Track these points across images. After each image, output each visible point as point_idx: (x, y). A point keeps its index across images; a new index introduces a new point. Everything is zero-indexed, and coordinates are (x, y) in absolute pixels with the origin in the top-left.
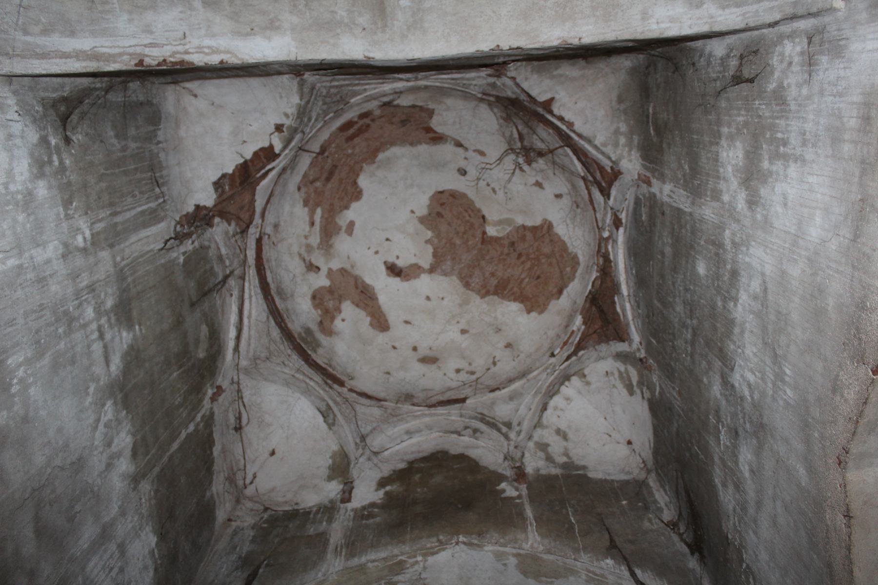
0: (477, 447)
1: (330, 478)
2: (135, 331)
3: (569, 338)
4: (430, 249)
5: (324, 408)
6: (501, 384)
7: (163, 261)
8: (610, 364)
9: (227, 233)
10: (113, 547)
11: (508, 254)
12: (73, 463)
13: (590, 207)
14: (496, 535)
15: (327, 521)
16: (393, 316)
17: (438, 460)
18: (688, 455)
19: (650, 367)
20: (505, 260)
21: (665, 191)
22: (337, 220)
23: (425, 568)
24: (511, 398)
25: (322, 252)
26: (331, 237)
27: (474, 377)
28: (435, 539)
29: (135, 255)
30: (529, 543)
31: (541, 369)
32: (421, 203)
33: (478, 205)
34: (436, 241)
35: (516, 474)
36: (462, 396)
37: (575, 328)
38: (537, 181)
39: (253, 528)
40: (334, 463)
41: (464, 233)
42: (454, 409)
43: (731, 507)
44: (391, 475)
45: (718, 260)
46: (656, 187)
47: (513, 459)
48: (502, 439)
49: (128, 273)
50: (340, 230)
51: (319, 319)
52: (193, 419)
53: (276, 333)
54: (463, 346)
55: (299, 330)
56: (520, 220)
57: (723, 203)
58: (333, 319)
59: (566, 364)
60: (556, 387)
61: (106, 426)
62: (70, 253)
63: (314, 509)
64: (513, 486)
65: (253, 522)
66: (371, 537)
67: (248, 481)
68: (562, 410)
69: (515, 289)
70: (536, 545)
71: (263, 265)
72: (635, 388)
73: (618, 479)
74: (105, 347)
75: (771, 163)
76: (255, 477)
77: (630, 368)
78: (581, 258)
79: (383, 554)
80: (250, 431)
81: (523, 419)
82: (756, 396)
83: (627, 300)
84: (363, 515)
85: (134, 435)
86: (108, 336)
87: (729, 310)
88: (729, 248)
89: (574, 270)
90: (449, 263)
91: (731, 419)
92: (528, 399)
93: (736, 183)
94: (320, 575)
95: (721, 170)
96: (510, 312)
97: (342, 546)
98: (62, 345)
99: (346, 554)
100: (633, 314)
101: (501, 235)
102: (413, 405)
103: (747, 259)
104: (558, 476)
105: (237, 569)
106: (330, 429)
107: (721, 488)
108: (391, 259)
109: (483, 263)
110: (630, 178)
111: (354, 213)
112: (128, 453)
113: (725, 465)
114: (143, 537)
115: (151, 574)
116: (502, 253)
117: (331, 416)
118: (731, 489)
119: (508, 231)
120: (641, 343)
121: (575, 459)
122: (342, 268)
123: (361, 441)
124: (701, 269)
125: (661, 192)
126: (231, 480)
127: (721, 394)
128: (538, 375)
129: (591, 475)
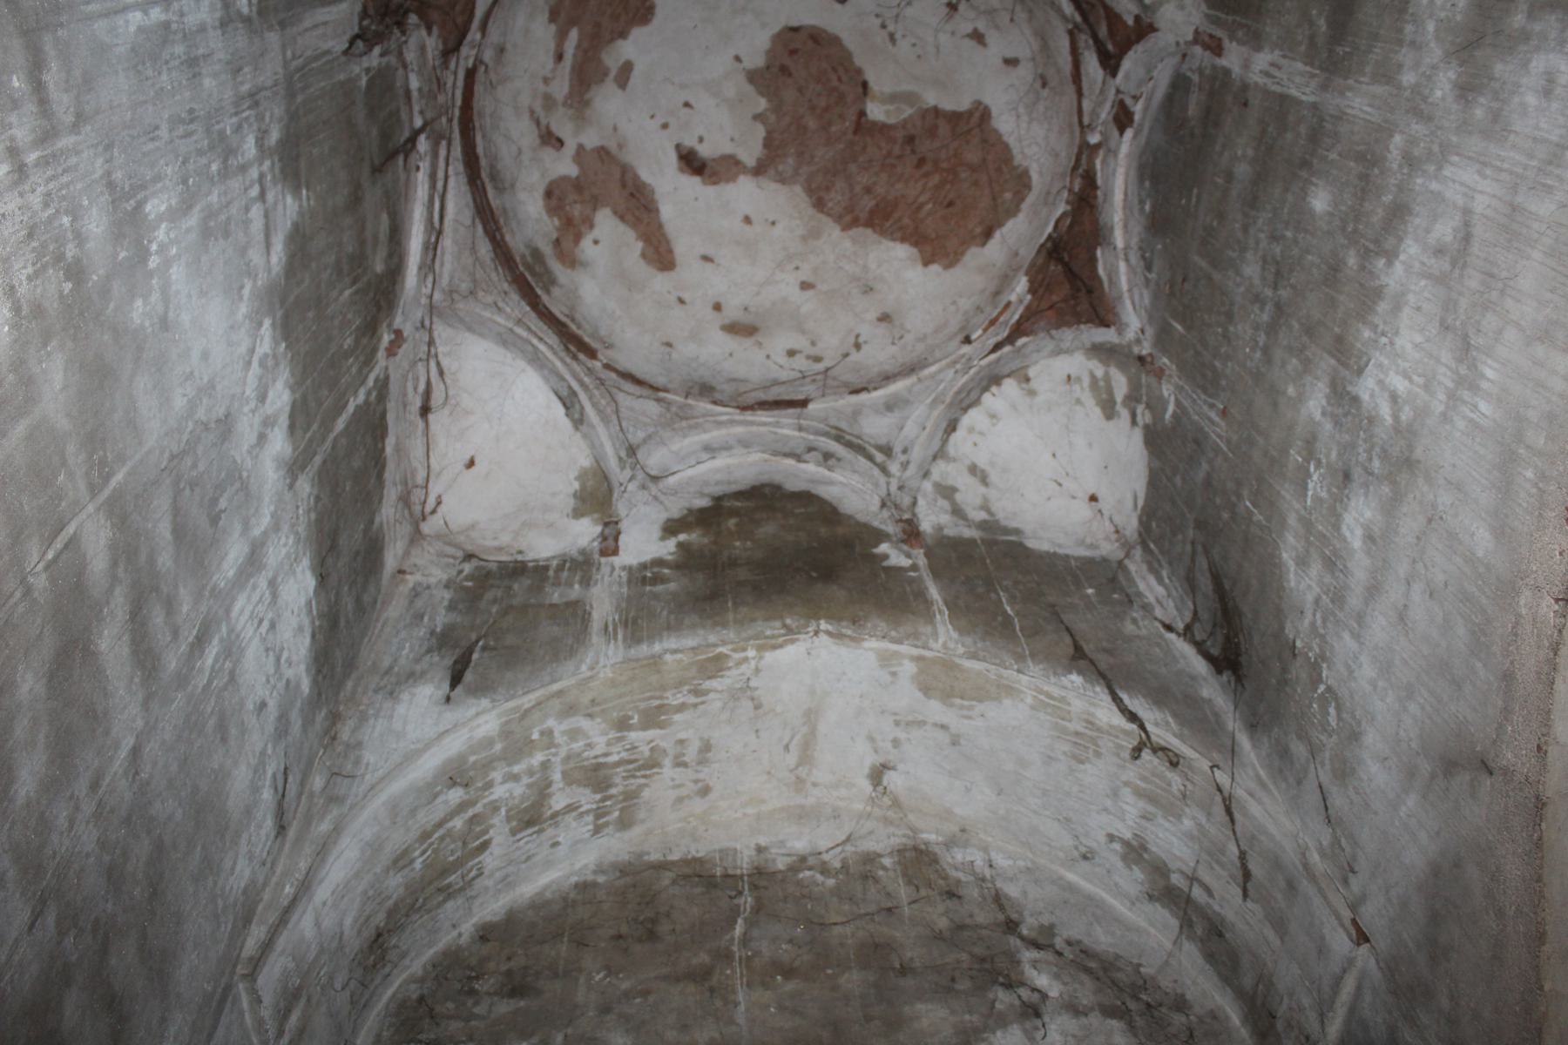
0: (831, 483)
1: (577, 514)
3: (1001, 313)
4: (760, 131)
5: (565, 393)
6: (869, 382)
7: (342, 77)
8: (1078, 364)
10: (262, 582)
11: (900, 157)
12: (218, 421)
13: (1071, 89)
14: (882, 626)
15: (581, 583)
16: (684, 247)
18: (1226, 515)
19: (1162, 371)
20: (894, 166)
21: (1255, 65)
23: (757, 670)
24: (890, 406)
25: (570, 112)
27: (820, 367)
28: (778, 624)
29: (309, 53)
30: (941, 641)
31: (944, 362)
32: (756, 46)
33: (859, 60)
34: (772, 118)
35: (904, 531)
36: (801, 397)
37: (1013, 298)
39: (447, 586)
40: (583, 488)
41: (826, 109)
42: (787, 417)
43: (1310, 598)
45: (1365, 186)
46: (1233, 58)
47: (897, 507)
48: (876, 472)
50: (606, 74)
51: (555, 236)
52: (363, 382)
53: (485, 249)
54: (804, 310)
55: (522, 248)
56: (931, 98)
57: (1399, 87)
58: (578, 238)
59: (993, 357)
60: (973, 396)
61: (262, 364)
62: (231, 21)
63: (555, 563)
64: (900, 550)
65: (445, 577)
67: (428, 509)
68: (981, 433)
69: (906, 221)
70: (952, 645)
71: (471, 120)
72: (1119, 407)
74: (266, 216)
75: (1531, 16)
76: (439, 503)
79: (690, 642)
81: (913, 442)
82: (1406, 415)
83: (1122, 256)
84: (644, 578)
85: (293, 390)
86: (270, 196)
87: (1371, 273)
88: (1395, 166)
89: (1019, 197)
90: (790, 161)
91: (1339, 454)
92: (918, 412)
94: (584, 668)
95: (1409, 28)
96: (893, 260)
100: (1129, 281)
101: (892, 121)
102: (715, 403)
103: (1434, 186)
105: (429, 651)
106: (577, 429)
108: (689, 142)
109: (853, 168)
110: (1171, 39)
111: (634, 47)
112: (284, 421)
113: (1307, 524)
114: (299, 575)
115: (308, 640)
116: (889, 154)
118: (1316, 568)
119: (905, 115)
120: (1143, 331)
121: (1000, 516)
122: (602, 148)
124: (1320, 202)
125: (1246, 65)
126: (405, 500)
127: (1324, 414)
128: (940, 371)
129: (1031, 544)
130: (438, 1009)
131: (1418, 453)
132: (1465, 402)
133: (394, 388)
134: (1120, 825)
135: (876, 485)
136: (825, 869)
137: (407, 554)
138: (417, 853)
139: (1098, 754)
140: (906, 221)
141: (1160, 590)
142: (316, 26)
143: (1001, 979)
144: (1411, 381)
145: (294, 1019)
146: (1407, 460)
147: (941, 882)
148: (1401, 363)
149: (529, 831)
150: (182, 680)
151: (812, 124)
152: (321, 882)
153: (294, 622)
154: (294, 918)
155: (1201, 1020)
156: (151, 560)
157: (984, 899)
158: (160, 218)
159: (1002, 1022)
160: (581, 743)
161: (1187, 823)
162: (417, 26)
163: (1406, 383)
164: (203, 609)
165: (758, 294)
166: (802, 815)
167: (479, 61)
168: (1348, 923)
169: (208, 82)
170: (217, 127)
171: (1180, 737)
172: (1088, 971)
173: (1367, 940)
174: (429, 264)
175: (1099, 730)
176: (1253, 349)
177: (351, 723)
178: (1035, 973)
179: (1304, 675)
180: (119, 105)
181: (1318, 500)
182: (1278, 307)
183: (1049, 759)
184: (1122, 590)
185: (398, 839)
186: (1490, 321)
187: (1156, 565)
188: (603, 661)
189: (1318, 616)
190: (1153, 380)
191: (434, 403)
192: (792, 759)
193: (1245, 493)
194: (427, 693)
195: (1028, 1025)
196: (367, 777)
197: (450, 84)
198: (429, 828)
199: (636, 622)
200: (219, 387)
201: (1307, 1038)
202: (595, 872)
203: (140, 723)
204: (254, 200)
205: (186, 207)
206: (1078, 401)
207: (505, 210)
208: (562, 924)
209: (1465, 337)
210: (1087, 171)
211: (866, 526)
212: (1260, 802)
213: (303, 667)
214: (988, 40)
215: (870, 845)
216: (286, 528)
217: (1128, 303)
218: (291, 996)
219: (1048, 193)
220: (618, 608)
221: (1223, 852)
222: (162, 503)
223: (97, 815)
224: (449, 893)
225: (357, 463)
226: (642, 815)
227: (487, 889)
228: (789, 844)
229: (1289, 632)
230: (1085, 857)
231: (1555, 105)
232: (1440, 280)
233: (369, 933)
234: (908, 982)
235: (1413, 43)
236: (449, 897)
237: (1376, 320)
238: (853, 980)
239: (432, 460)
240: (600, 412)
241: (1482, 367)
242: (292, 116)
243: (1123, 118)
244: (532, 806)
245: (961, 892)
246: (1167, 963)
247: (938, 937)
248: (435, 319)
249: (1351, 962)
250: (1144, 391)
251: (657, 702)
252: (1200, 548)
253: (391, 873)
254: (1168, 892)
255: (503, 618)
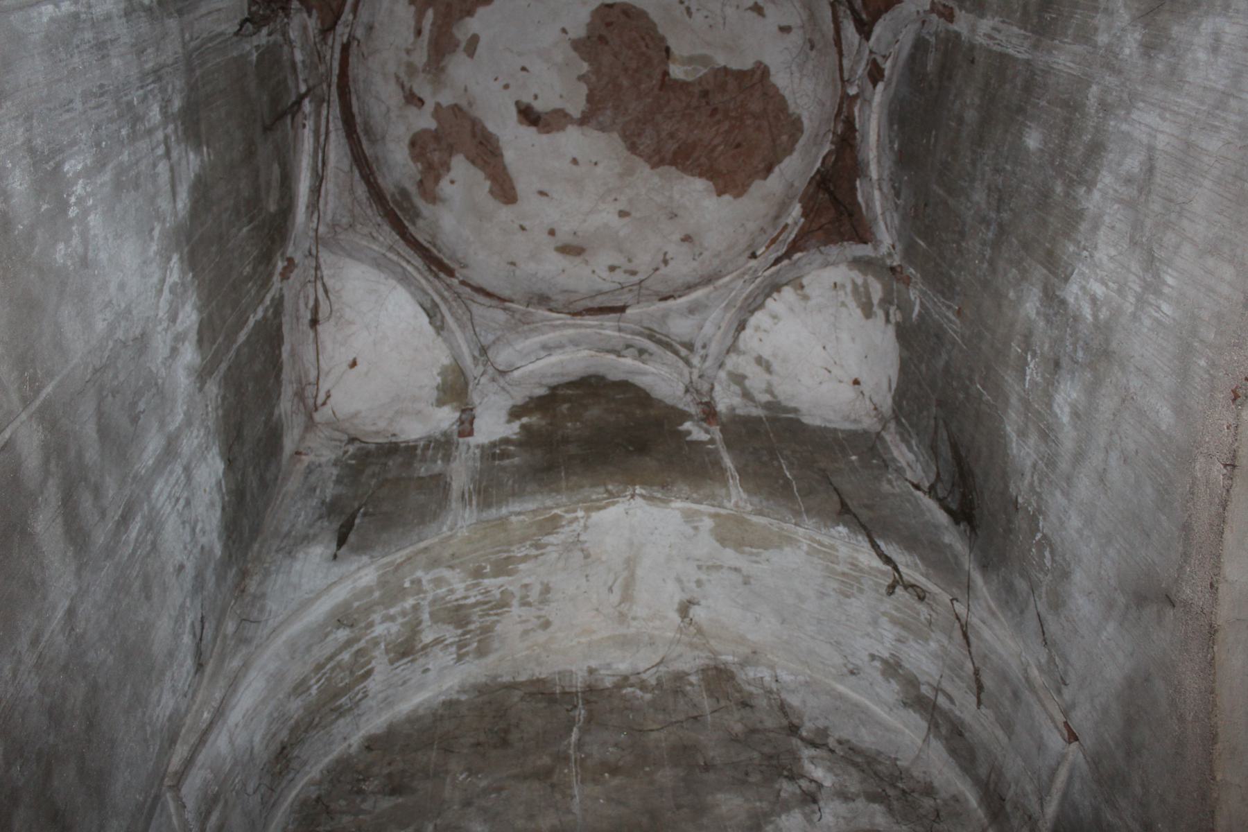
0: (645, 373)
1: (440, 403)
2: (202, 155)
4: (584, 90)
5: (428, 305)
6: (675, 291)
7: (235, 54)
8: (841, 273)
9: (305, 28)
11: (697, 108)
12: (135, 339)
14: (686, 489)
15: (443, 459)
16: (524, 184)
17: (591, 387)
18: (961, 396)
19: (909, 278)
21: (979, 29)
22: (454, 31)
23: (586, 527)
24: (692, 310)
25: (429, 77)
26: (443, 55)
27: (636, 279)
28: (601, 490)
29: (205, 35)
31: (735, 274)
32: (578, 20)
33: (661, 31)
34: (594, 78)
35: (704, 412)
36: (620, 304)
37: (790, 221)
38: (756, 3)
39: (335, 464)
40: (444, 382)
42: (609, 321)
43: (1029, 463)
44: (527, 403)
47: (697, 391)
48: (681, 364)
49: (196, 62)
50: (457, 45)
51: (419, 177)
52: (262, 301)
53: (361, 190)
54: (621, 234)
55: (392, 189)
56: (721, 60)
57: (1095, 46)
58: (437, 179)
59: (774, 269)
60: (759, 300)
61: (172, 291)
62: (134, 11)
63: (422, 443)
64: (701, 427)
65: (333, 457)
66: (510, 482)
67: (319, 401)
70: (741, 504)
71: (347, 86)
72: (875, 309)
73: (843, 427)
74: (172, 170)
76: (328, 397)
77: (871, 279)
78: (806, 122)
79: (531, 506)
80: (325, 329)
81: (710, 340)
82: (1104, 314)
83: (876, 186)
84: (494, 455)
85: (200, 311)
86: (175, 154)
87: (1074, 198)
89: (794, 139)
90: (609, 112)
92: (715, 314)
93: (1127, 17)
94: (445, 529)
96: (694, 194)
97: (470, 493)
98: (125, 157)
99: (478, 505)
101: (690, 79)
102: (551, 310)
103: (1124, 127)
104: (761, 418)
105: (321, 517)
106: (438, 334)
107: (1014, 437)
108: (527, 99)
109: (659, 117)
110: (913, 9)
111: (477, 23)
112: (193, 336)
113: (1026, 403)
114: (210, 460)
115: (219, 513)
117: (439, 316)
118: (1033, 439)
119: (701, 74)
120: (894, 247)
121: (781, 398)
122: (456, 105)
123: (481, 355)
124: (1033, 141)
125: (973, 30)
126: (300, 395)
127: (1038, 313)
130: (333, 806)
131: (1114, 345)
132: (1151, 304)
133: (288, 305)
134: (879, 647)
135: (681, 374)
136: (643, 686)
137: (302, 439)
138: (313, 681)
139: (861, 591)
140: (703, 160)
141: (911, 456)
142: (210, 13)
143: (785, 773)
144: (1107, 286)
145: (214, 819)
146: (1105, 351)
147: (737, 695)
148: (1099, 275)
149: (405, 660)
150: (109, 552)
151: (625, 83)
152: (233, 708)
153: (207, 499)
154: (212, 738)
155: (946, 803)
156: (80, 455)
157: (771, 706)
158: (78, 175)
159: (786, 807)
160: (444, 590)
161: (933, 645)
162: (299, 10)
163: (1104, 289)
164: (127, 492)
165: (585, 221)
166: (625, 643)
167: (352, 37)
168: (1061, 726)
169: (115, 62)
170: (125, 99)
171: (927, 576)
172: (855, 765)
173: (1076, 739)
174: (313, 206)
175: (861, 571)
176: (981, 262)
177: (257, 578)
178: (813, 767)
179: (1025, 526)
180: (36, 84)
181: (1035, 384)
182: (1001, 227)
183: (822, 595)
184: (880, 456)
185: (297, 671)
186: (1170, 238)
187: (906, 436)
188: (461, 523)
189: (1035, 478)
190: (902, 287)
191: (320, 315)
192: (615, 598)
193: (976, 378)
194: (318, 551)
195: (807, 810)
196: (270, 622)
197: (328, 57)
198: (322, 660)
199: (488, 490)
200: (135, 312)
201: (1030, 817)
202: (458, 692)
203: (74, 589)
204: (160, 158)
205: (100, 165)
206: (843, 304)
207: (377, 158)
208: (432, 734)
209: (1150, 252)
210: (847, 117)
211: (673, 408)
212: (990, 628)
213: (215, 535)
214: (766, 11)
215: (680, 666)
216: (197, 423)
217: (882, 224)
218: (210, 801)
219: (817, 135)
220: (472, 479)
221: (961, 668)
222: (87, 408)
223: (38, 666)
224: (340, 712)
225: (257, 367)
226: (496, 645)
227: (371, 708)
228: (614, 666)
229: (1013, 490)
230: (852, 673)
231: (1220, 60)
232: (1130, 204)
233: (275, 746)
234: (711, 777)
235: (1106, 10)
236: (341, 715)
237: (1079, 237)
238: (666, 776)
239: (322, 362)
240: (457, 320)
241: (1162, 275)
242: (192, 88)
243: (875, 74)
244: (407, 641)
245: (753, 702)
246: (918, 757)
247: (735, 739)
248: (320, 248)
249: (1064, 756)
250: (895, 294)
251: (505, 555)
252: (941, 422)
253: (292, 698)
254: (918, 700)
255: (380, 490)
